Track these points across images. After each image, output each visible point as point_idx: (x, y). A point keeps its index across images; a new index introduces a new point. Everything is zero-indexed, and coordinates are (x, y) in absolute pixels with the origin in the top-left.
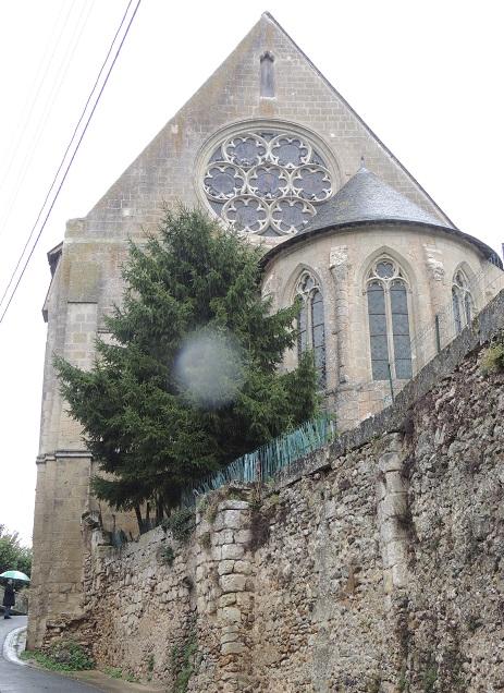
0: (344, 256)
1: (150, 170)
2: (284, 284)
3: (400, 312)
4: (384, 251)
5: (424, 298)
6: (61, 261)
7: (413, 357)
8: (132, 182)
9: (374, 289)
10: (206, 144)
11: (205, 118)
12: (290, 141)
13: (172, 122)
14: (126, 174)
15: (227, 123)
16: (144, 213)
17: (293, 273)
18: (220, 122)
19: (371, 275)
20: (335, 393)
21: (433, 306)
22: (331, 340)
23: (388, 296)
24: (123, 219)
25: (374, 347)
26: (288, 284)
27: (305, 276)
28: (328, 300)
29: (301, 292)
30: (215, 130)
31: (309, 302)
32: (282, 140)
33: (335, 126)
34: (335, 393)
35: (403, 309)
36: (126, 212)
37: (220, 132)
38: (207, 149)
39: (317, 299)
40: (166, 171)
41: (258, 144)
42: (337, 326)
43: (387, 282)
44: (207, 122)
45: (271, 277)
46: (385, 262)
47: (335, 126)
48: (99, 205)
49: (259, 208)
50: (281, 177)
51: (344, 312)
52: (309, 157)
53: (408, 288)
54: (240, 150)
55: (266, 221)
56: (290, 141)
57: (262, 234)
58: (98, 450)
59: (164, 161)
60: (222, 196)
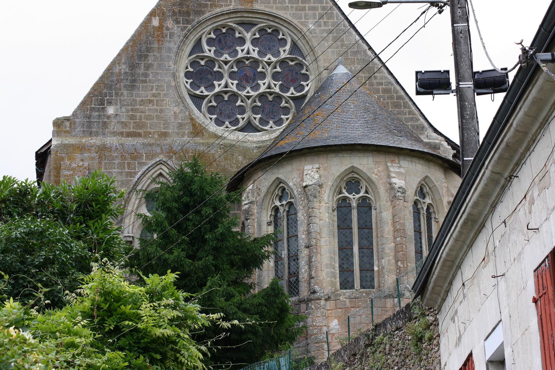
0: (317, 176)
1: (133, 67)
2: (262, 195)
3: (366, 227)
4: (353, 170)
5: (387, 215)
6: (51, 160)
7: (376, 268)
8: (115, 79)
9: (342, 207)
10: (186, 37)
11: (185, 9)
12: (269, 31)
13: (152, 14)
14: (109, 71)
15: (207, 15)
16: (128, 111)
17: (271, 185)
18: (199, 13)
19: (341, 192)
20: (307, 301)
21: (394, 222)
22: (304, 253)
23: (355, 213)
24: (109, 117)
25: (341, 259)
26: (266, 196)
27: (281, 190)
28: (301, 216)
29: (278, 203)
30: (195, 23)
31: (285, 214)
32: (261, 30)
33: (314, 15)
34: (307, 301)
35: (368, 224)
36: (111, 110)
37: (200, 24)
38: (188, 42)
39: (292, 211)
40: (148, 67)
41: (237, 35)
42: (309, 240)
43: (354, 198)
44: (188, 14)
45: (251, 187)
46: (352, 181)
47: (314, 16)
48: (84, 103)
49: (239, 103)
50: (260, 70)
51: (314, 228)
52: (288, 47)
53: (373, 205)
54: (220, 41)
55: (246, 116)
56: (269, 31)
57: (242, 130)
58: (20, 191)
59: (146, 56)
60: (202, 91)
